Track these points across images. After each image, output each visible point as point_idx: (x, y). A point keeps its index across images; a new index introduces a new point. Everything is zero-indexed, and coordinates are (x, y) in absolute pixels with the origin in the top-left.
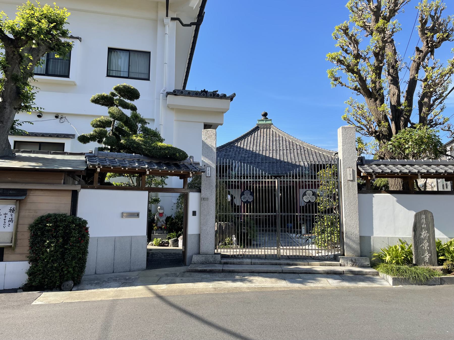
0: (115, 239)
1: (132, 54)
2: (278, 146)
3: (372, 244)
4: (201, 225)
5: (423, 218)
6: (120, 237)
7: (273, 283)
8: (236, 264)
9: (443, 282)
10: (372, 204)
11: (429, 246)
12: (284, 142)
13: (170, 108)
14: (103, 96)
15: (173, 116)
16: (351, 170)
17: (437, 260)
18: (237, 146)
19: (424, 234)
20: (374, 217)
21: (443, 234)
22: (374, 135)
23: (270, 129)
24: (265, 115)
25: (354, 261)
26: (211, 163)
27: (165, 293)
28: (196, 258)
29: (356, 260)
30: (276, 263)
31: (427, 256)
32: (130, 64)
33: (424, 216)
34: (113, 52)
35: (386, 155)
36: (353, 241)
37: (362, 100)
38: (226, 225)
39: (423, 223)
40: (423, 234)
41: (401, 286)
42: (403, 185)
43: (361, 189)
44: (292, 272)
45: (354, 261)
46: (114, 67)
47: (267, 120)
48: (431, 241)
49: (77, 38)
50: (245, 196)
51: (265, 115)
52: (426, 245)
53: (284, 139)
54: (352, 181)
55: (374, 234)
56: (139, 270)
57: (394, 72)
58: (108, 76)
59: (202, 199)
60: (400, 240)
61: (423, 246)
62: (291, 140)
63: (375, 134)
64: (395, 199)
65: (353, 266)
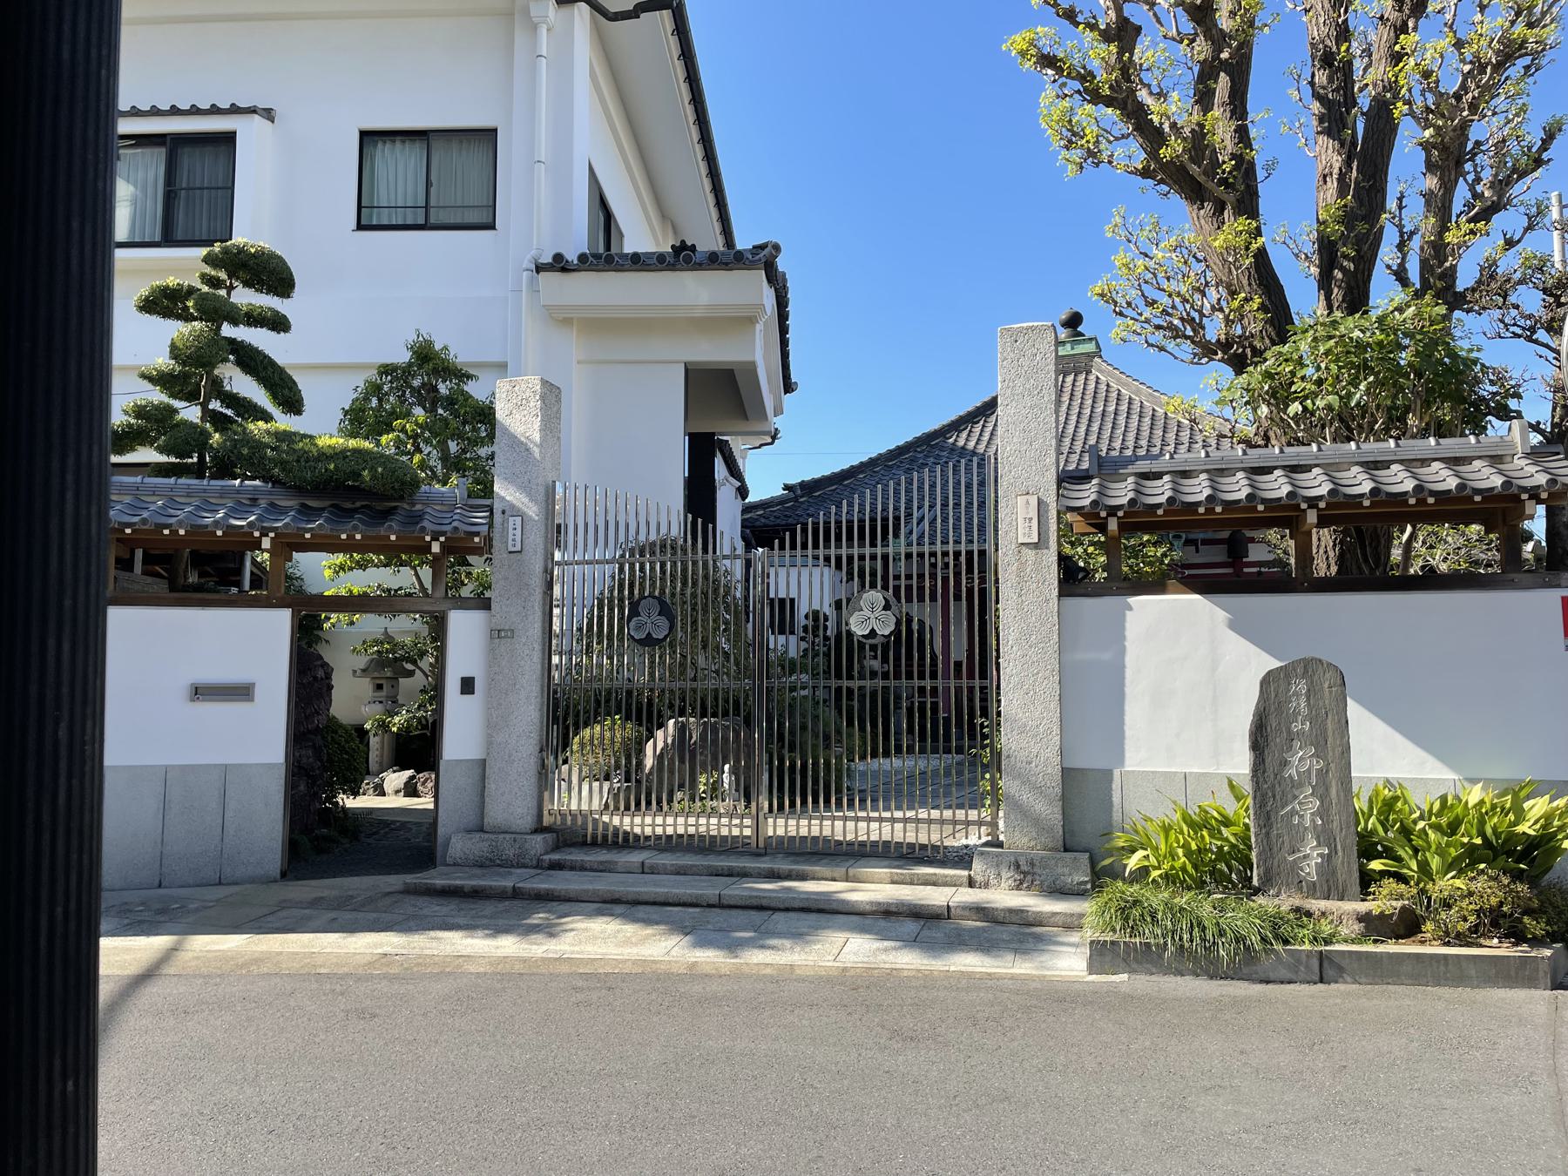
0: (166, 774)
1: (435, 145)
2: (1106, 434)
3: (1116, 799)
4: (493, 726)
5: (1296, 694)
6: (184, 769)
7: (627, 942)
8: (592, 870)
9: (1330, 972)
10: (1124, 638)
11: (1323, 812)
12: (1135, 418)
13: (563, 319)
14: (167, 287)
15: (571, 346)
16: (1034, 501)
17: (1356, 875)
18: (954, 447)
19: (1301, 761)
20: (1128, 690)
21: (1438, 764)
22: (1220, 355)
23: (1088, 372)
24: (1074, 321)
25: (1024, 868)
26: (526, 500)
27: (1034, 985)
28: (459, 846)
29: (1032, 864)
30: (730, 868)
31: (1311, 857)
32: (433, 178)
33: (1302, 686)
34: (380, 145)
35: (1271, 434)
36: (1038, 789)
37: (1184, 223)
38: (705, 730)
39: (1296, 713)
40: (1295, 760)
41: (1125, 976)
42: (1341, 560)
43: (1072, 579)
44: (755, 902)
45: (1024, 868)
46: (383, 196)
47: (1079, 342)
48: (1333, 792)
49: (252, 111)
50: (643, 618)
51: (1074, 321)
52: (1307, 808)
53: (1136, 407)
54: (1036, 546)
55: (1128, 761)
56: (252, 880)
57: (1330, 80)
58: (360, 227)
59: (497, 634)
60: (1231, 786)
61: (1293, 812)
62: (1161, 411)
63: (1224, 353)
64: (1221, 615)
65: (1018, 888)
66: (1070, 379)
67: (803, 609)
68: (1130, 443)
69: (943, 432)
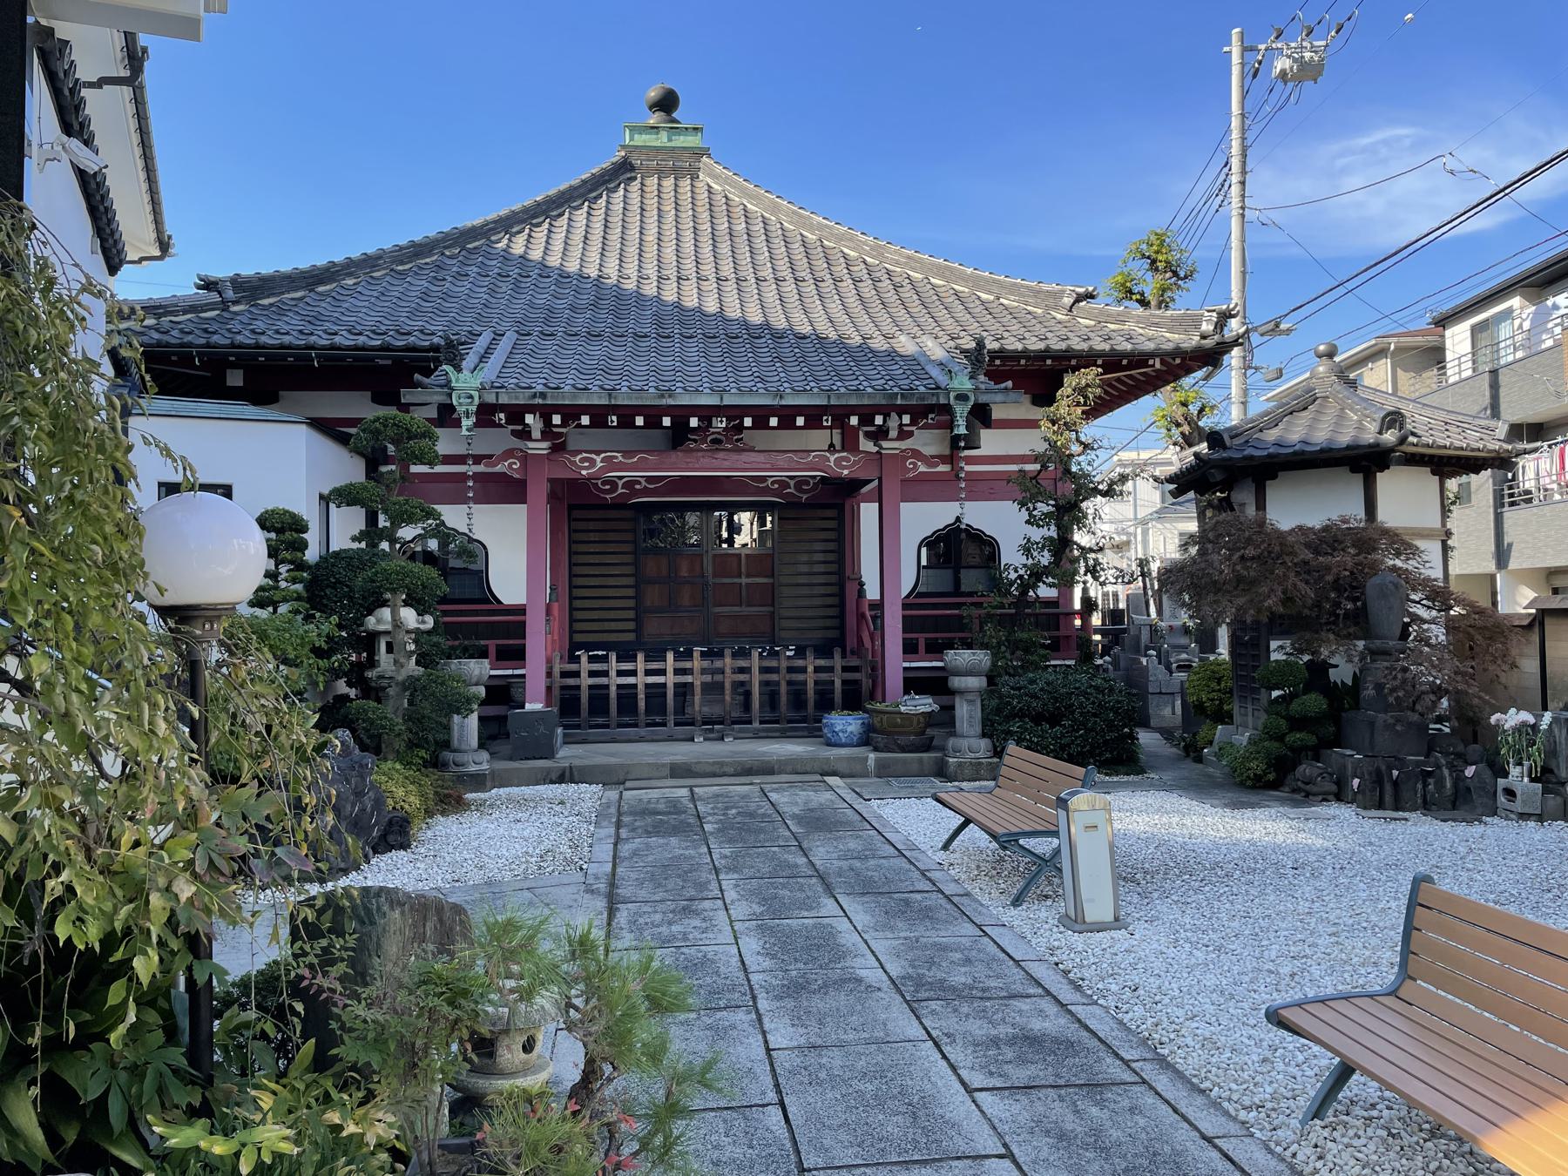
18: (506, 256)
24: (667, 103)
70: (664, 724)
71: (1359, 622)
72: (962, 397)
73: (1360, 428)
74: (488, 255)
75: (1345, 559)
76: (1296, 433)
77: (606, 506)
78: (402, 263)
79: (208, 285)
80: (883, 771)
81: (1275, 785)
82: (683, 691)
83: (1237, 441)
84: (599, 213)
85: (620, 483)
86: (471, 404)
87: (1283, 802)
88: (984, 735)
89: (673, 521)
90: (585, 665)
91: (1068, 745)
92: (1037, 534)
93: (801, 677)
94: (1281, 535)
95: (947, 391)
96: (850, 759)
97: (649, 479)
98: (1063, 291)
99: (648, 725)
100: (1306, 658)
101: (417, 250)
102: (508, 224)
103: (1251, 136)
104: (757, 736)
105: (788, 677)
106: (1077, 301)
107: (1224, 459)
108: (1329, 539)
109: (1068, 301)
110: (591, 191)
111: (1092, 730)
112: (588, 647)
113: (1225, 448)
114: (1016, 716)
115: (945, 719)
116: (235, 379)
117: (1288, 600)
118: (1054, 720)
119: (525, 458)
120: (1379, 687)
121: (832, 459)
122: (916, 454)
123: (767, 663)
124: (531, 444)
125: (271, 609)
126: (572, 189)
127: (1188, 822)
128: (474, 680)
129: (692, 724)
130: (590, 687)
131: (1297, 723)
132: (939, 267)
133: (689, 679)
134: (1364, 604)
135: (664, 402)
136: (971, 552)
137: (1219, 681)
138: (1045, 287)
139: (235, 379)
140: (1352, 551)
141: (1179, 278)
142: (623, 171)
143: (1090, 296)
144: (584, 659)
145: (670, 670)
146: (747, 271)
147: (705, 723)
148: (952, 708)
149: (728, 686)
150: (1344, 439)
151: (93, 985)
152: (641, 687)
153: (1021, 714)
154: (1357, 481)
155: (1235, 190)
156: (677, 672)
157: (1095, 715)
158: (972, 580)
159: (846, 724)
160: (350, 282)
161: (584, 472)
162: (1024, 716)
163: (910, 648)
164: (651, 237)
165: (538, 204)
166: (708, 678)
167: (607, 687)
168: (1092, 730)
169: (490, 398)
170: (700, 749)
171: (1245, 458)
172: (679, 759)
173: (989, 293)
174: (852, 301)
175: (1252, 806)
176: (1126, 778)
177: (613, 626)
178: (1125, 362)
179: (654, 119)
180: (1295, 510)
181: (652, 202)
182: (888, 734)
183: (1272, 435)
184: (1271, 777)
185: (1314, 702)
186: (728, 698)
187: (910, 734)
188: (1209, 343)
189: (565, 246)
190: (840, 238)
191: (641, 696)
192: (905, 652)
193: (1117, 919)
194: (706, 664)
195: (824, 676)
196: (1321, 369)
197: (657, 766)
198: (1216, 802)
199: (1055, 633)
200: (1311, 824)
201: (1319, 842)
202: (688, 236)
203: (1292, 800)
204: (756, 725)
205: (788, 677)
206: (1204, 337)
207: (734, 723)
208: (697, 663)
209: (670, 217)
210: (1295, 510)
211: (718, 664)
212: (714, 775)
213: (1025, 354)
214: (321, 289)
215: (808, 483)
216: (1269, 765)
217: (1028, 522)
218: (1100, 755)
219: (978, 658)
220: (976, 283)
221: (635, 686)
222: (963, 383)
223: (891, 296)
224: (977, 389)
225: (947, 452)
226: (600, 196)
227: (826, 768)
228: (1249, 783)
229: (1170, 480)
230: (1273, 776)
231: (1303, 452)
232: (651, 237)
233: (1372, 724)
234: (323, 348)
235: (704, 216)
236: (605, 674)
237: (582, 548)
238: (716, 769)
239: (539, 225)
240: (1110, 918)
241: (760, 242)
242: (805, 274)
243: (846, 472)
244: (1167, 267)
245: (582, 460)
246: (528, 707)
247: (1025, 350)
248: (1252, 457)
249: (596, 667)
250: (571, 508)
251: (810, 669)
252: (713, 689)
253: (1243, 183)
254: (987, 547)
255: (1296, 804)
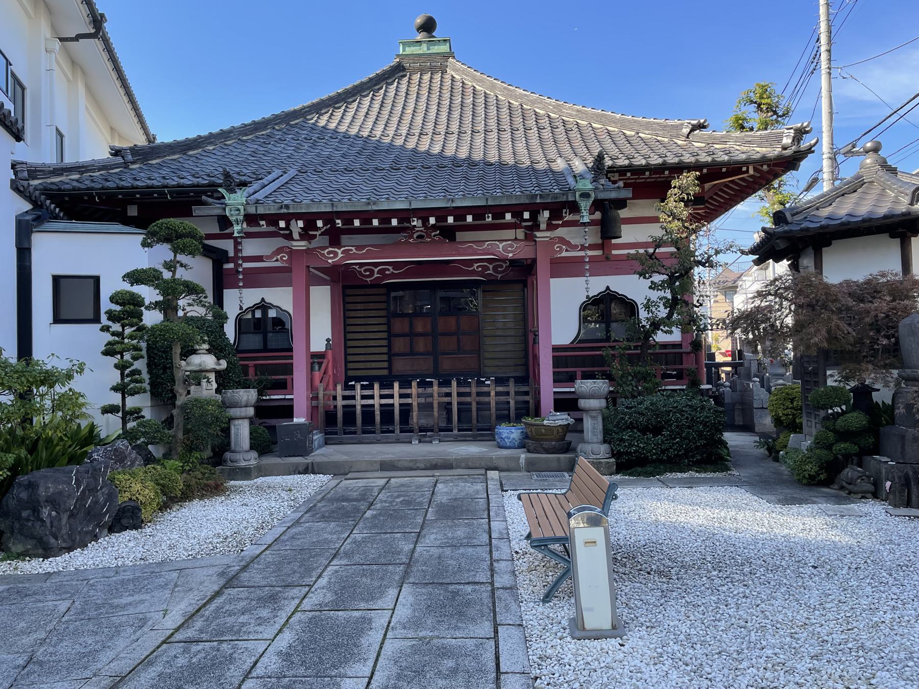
18: (314, 127)
23: (444, 72)
24: (428, 26)
53: (492, 101)
62: (515, 103)
66: (427, 77)
67: (769, 225)
68: (404, 131)
69: (295, 114)
70: (393, 432)
71: (894, 354)
72: (585, 195)
73: (896, 201)
74: (302, 128)
75: (881, 305)
76: (844, 209)
77: (366, 286)
78: (246, 135)
79: (116, 152)
80: (531, 467)
81: (827, 483)
82: (406, 411)
83: (797, 218)
84: (379, 99)
85: (376, 270)
86: (238, 214)
87: (829, 498)
88: (605, 441)
89: (472, 301)
90: (358, 392)
91: (667, 450)
92: (655, 295)
93: (486, 399)
94: (827, 286)
95: (575, 191)
96: (507, 458)
97: (395, 265)
98: (682, 124)
99: (383, 432)
100: (853, 384)
101: (256, 127)
102: (318, 108)
103: (837, 23)
104: (457, 439)
105: (478, 399)
106: (692, 130)
107: (785, 232)
108: (869, 290)
109: (686, 131)
110: (375, 85)
111: (685, 438)
112: (358, 379)
113: (787, 223)
114: (628, 427)
115: (577, 428)
116: (133, 211)
117: (831, 337)
118: (657, 431)
119: (292, 253)
120: (909, 407)
121: (501, 246)
122: (562, 240)
123: (463, 390)
124: (294, 243)
125: (119, 356)
126: (362, 84)
127: (740, 517)
128: (244, 403)
129: (412, 431)
130: (344, 406)
131: (845, 435)
132: (598, 115)
133: (409, 401)
134: (897, 339)
135: (369, 208)
136: (615, 309)
137: (792, 401)
138: (670, 122)
139: (133, 211)
140: (888, 298)
141: (779, 116)
142: (398, 71)
143: (701, 127)
144: (358, 387)
145: (396, 395)
146: (468, 128)
147: (421, 431)
148: (582, 420)
149: (436, 405)
150: (882, 211)
151: (129, 575)
152: (377, 407)
153: (631, 426)
154: (894, 247)
155: (824, 56)
156: (402, 396)
157: (689, 427)
158: (618, 331)
159: (510, 432)
160: (211, 148)
161: (330, 261)
162: (634, 428)
163: (558, 379)
164: (409, 111)
165: (339, 94)
166: (422, 400)
167: (354, 406)
168: (685, 438)
169: (252, 210)
170: (416, 449)
171: (802, 230)
172: (387, 457)
173: (632, 130)
174: (534, 141)
175: (800, 502)
176: (711, 475)
177: (373, 365)
178: (724, 170)
179: (420, 37)
180: (843, 268)
181: (414, 89)
182: (537, 440)
183: (825, 212)
184: (822, 477)
185: (857, 419)
186: (436, 414)
187: (551, 440)
188: (788, 152)
189: (351, 121)
190: (533, 102)
191: (377, 413)
192: (554, 381)
193: (614, 627)
194: (421, 390)
195: (502, 398)
196: (868, 161)
197: (372, 463)
198: (773, 498)
199: (680, 367)
200: (844, 521)
201: (846, 540)
202: (434, 108)
203: (836, 496)
204: (455, 432)
205: (478, 399)
206: (785, 148)
207: (441, 430)
208: (414, 390)
209: (424, 99)
210: (843, 268)
211: (429, 390)
212: (411, 469)
213: (648, 168)
214: (191, 153)
215: (501, 266)
216: (821, 468)
217: (650, 288)
218: (693, 457)
219: (601, 385)
220: (623, 124)
221: (373, 406)
222: (586, 185)
223: (562, 137)
224: (596, 188)
225: (600, 241)
226: (381, 88)
227: (490, 464)
228: (805, 481)
229: (753, 251)
230: (828, 476)
231: (849, 223)
232: (409, 111)
233: (903, 437)
234: (173, 186)
235: (447, 95)
236: (353, 398)
237: (352, 314)
238: (411, 465)
239: (339, 108)
240: (607, 626)
241: (480, 110)
242: (507, 127)
243: (511, 255)
244: (773, 112)
245: (329, 253)
246: (296, 420)
247: (648, 164)
248: (807, 229)
249: (348, 393)
250: (345, 287)
251: (493, 393)
252: (426, 407)
253: (829, 51)
254: (630, 307)
255: (839, 500)
